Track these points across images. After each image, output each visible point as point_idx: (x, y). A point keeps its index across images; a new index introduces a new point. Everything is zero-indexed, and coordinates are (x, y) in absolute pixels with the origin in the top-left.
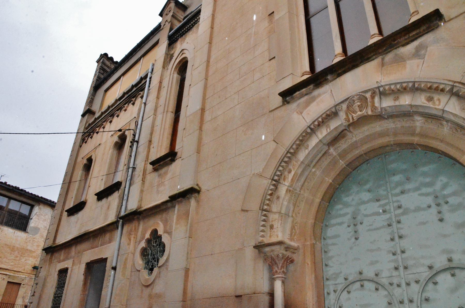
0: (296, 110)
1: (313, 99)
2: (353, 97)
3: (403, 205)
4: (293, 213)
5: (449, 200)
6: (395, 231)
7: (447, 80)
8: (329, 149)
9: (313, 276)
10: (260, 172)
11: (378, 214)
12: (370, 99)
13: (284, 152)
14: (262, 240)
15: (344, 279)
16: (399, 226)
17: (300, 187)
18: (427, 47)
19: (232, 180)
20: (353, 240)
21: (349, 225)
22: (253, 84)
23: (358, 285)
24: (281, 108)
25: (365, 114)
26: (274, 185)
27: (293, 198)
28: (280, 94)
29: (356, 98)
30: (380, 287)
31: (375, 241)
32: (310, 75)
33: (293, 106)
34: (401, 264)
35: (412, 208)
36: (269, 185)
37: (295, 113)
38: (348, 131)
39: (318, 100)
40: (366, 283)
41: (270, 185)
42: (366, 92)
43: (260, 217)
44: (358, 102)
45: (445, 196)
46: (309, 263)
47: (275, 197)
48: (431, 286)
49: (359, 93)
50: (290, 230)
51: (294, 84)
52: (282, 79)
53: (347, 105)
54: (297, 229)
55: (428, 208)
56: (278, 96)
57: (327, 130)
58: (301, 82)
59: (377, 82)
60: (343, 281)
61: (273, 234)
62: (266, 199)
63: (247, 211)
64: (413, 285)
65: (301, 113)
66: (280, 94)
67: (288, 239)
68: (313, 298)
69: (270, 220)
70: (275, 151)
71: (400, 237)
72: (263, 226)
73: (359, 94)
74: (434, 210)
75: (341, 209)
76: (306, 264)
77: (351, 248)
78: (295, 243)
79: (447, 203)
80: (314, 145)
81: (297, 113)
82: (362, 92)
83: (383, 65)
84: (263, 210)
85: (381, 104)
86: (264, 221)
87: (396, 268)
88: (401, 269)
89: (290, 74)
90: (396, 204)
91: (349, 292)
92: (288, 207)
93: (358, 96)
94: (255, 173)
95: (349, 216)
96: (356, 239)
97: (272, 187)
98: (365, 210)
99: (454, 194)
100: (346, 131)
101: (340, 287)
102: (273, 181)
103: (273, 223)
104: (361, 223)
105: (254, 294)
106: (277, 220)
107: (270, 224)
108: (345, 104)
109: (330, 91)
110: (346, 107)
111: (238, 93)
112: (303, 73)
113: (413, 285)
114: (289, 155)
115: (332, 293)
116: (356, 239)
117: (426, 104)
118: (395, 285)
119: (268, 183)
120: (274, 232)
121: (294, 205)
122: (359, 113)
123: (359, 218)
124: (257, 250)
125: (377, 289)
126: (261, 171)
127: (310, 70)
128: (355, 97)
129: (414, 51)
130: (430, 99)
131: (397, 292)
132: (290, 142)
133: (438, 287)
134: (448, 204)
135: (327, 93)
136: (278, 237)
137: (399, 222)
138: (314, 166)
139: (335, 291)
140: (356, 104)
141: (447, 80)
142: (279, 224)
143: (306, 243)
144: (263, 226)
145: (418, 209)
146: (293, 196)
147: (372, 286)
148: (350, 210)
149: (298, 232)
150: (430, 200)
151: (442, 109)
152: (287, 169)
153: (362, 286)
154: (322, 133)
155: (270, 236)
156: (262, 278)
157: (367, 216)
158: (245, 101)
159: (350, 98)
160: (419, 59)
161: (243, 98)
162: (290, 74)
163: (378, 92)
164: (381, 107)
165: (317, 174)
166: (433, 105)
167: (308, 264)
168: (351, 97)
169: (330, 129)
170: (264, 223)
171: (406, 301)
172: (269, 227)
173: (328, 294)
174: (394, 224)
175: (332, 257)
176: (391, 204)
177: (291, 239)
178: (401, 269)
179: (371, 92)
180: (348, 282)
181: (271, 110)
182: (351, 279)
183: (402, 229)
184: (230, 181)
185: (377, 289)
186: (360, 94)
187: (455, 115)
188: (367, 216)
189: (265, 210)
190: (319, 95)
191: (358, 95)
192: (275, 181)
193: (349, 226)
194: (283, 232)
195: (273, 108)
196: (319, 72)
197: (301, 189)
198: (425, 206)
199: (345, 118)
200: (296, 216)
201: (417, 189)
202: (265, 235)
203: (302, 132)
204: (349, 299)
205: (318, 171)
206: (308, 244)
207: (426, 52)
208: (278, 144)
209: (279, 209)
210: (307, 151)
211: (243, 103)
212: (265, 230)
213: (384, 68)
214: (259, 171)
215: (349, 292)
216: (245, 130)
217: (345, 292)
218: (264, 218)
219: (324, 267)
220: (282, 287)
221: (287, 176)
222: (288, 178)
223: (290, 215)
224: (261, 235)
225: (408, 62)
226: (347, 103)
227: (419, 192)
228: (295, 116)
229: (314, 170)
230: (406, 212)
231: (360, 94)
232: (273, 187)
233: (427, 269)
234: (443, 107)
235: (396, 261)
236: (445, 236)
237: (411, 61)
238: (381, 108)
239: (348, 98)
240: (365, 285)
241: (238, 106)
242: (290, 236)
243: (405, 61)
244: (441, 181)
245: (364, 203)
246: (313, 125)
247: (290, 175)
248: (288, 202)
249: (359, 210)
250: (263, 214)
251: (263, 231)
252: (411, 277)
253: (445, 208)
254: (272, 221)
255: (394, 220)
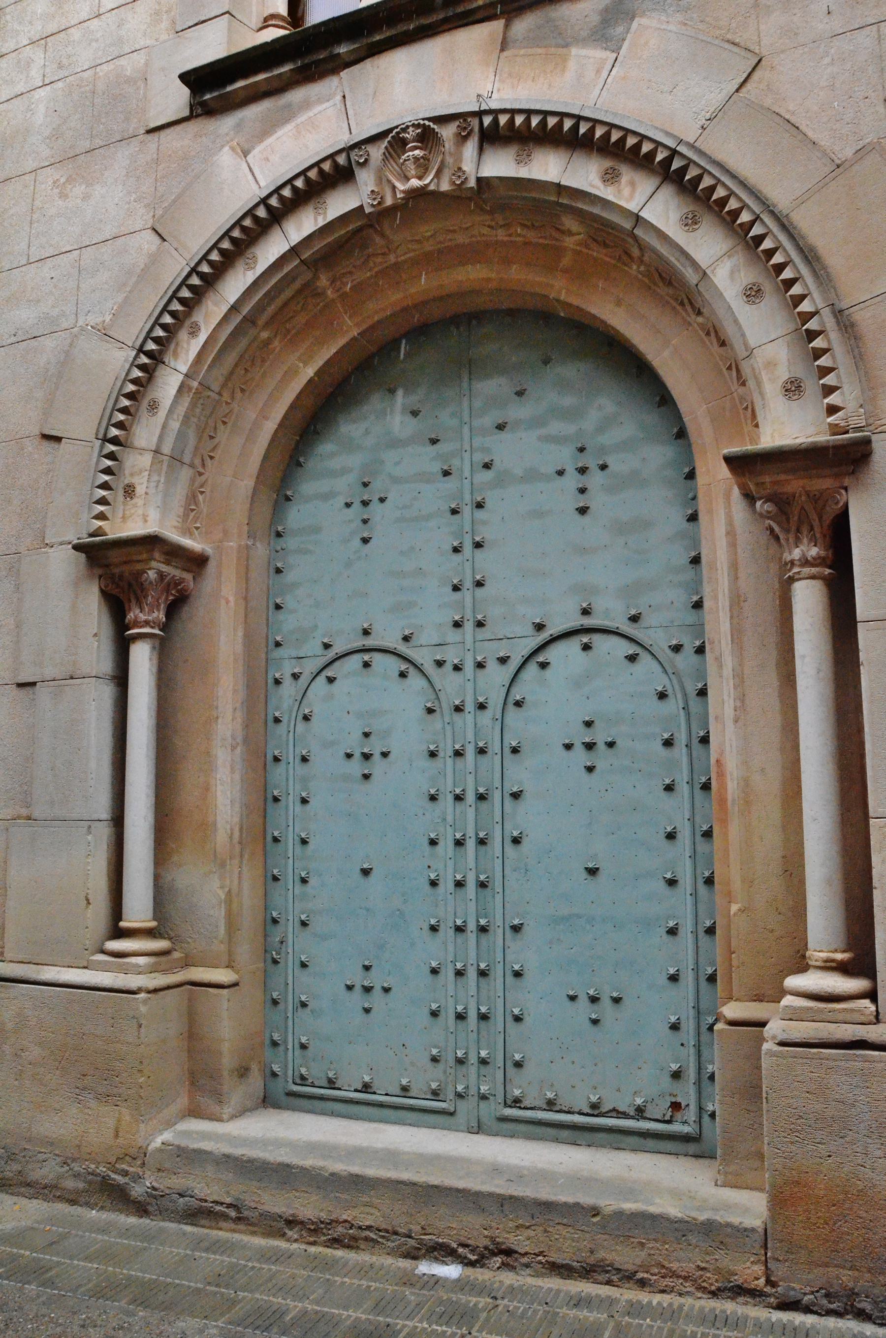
0: (232, 140)
1: (287, 116)
2: (404, 130)
3: (497, 464)
4: (195, 455)
5: (610, 460)
6: (467, 527)
7: (662, 130)
8: (316, 277)
9: (240, 633)
10: (104, 321)
11: (423, 477)
12: (452, 143)
13: (182, 270)
14: (100, 527)
15: (322, 647)
16: (480, 514)
17: (221, 379)
18: (632, 19)
19: (14, 339)
20: (357, 542)
21: (348, 501)
22: (96, 20)
23: (356, 661)
24: (185, 124)
25: (432, 187)
26: (142, 367)
27: (198, 410)
28: (184, 77)
29: (411, 134)
30: (412, 671)
31: (412, 548)
32: (287, 32)
33: (227, 123)
34: (469, 614)
35: (518, 471)
36: (127, 366)
37: (227, 148)
38: (376, 231)
39: (302, 118)
40: (377, 659)
41: (132, 365)
42: (442, 120)
43: (95, 460)
44: (416, 148)
45: (602, 450)
46: (231, 599)
47: (145, 403)
48: (532, 668)
49: (423, 119)
50: (183, 503)
51: (230, 53)
52: (196, 24)
53: (384, 153)
54: (204, 502)
55: (556, 475)
56: (178, 81)
57: (316, 219)
58: (255, 48)
59: (479, 96)
60: (319, 650)
61: (133, 511)
62: (118, 407)
63: (58, 439)
64: (492, 666)
65: (245, 153)
66: (184, 77)
67: (175, 527)
68: (235, 691)
69: (127, 472)
70: (154, 259)
71: (478, 545)
72: (105, 486)
73: (422, 122)
74: (572, 480)
75: (332, 455)
76: (223, 602)
77: (349, 564)
78: (194, 539)
79: (603, 467)
80: (272, 259)
81: (233, 149)
82: (429, 119)
83: (504, 46)
84: (106, 440)
85: (480, 167)
86: (108, 471)
87: (457, 625)
88: (469, 626)
89: (222, 14)
90: (480, 458)
91: (331, 680)
92: (181, 436)
93: (419, 131)
94: (87, 325)
95: (352, 478)
96: (365, 541)
97: (137, 373)
98: (397, 464)
99: (625, 446)
100: (371, 231)
101: (309, 668)
102: (142, 355)
103: (135, 480)
104: (382, 500)
105: (72, 678)
106: (147, 473)
107: (126, 482)
108: (379, 146)
109: (339, 98)
110: (381, 158)
111: (43, 42)
112: (266, 20)
113: (492, 666)
114: (195, 281)
115: (288, 681)
116: (365, 541)
117: (598, 188)
118: (448, 667)
119: (126, 361)
120: (135, 506)
121: (201, 432)
122: (415, 183)
123: (378, 486)
124: (83, 555)
125: (403, 675)
126: (108, 318)
127: (289, 15)
128: (411, 129)
129: (595, 19)
130: (610, 177)
131: (448, 682)
132: (201, 241)
133: (548, 672)
134: (607, 471)
135: (331, 103)
136: (146, 521)
137: (480, 506)
138: (267, 325)
139: (296, 676)
140: (411, 153)
141: (662, 130)
142: (153, 484)
143: (226, 544)
144: (105, 486)
145: (531, 476)
146: (199, 406)
147: (395, 665)
148: (355, 461)
149: (205, 510)
150: (565, 456)
151: (636, 212)
152: (187, 323)
153: (366, 665)
154: (299, 229)
155: (124, 518)
156: (95, 635)
157: (396, 480)
158: (68, 80)
159: (396, 130)
160: (606, 49)
161: (60, 66)
162: (222, 14)
163: (476, 129)
164: (479, 175)
165: (275, 349)
166: (615, 196)
167: (227, 602)
168: (397, 127)
169: (324, 219)
170: (106, 478)
171: (470, 706)
172: (121, 492)
173: (277, 682)
174: (467, 511)
175: (294, 585)
176: (467, 456)
177: (187, 532)
178: (469, 626)
179: (457, 123)
180: (331, 654)
181: (152, 125)
182: (339, 648)
183: (484, 523)
184: (9, 341)
185: (403, 675)
186: (427, 123)
187: (663, 236)
188: (396, 480)
189: (115, 441)
190: (306, 105)
191: (417, 126)
192: (149, 354)
193: (348, 505)
194: (164, 509)
195: (159, 123)
196: (315, 27)
197: (224, 386)
198: (551, 470)
199: (372, 191)
200: (203, 465)
201: (537, 422)
202: (109, 515)
203: (240, 214)
204: (330, 697)
205: (278, 339)
206: (232, 547)
207: (627, 33)
208: (164, 240)
209: (155, 439)
210: (251, 277)
211: (60, 84)
212: (110, 499)
213: (505, 54)
214: (101, 319)
215: (331, 680)
216: (63, 180)
217: (321, 680)
218: (109, 463)
219: (270, 613)
220: (150, 659)
221: (185, 346)
222: (187, 351)
223: (187, 459)
224: (96, 512)
225: (574, 51)
226: (384, 146)
227: (543, 431)
228: (226, 158)
229: (265, 335)
230: (501, 482)
231: (427, 123)
232: (140, 374)
233: (530, 630)
234: (639, 208)
235: (461, 605)
236: (583, 551)
237: (584, 52)
238: (479, 180)
239: (390, 130)
240: (373, 664)
241: (42, 93)
242: (180, 520)
243: (566, 46)
244: (600, 408)
245: (394, 443)
246: (276, 196)
247: (193, 341)
248: (182, 424)
249: (382, 462)
250: (105, 451)
251: (102, 501)
252: (490, 651)
253: (595, 479)
254: (132, 475)
255: (467, 497)
